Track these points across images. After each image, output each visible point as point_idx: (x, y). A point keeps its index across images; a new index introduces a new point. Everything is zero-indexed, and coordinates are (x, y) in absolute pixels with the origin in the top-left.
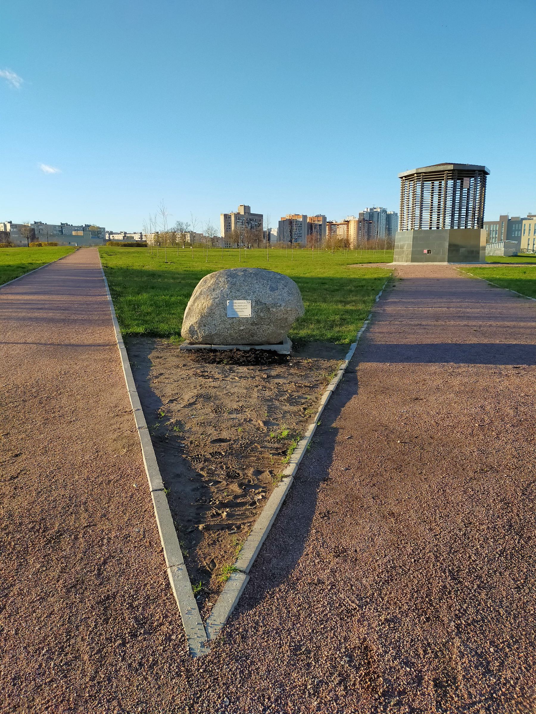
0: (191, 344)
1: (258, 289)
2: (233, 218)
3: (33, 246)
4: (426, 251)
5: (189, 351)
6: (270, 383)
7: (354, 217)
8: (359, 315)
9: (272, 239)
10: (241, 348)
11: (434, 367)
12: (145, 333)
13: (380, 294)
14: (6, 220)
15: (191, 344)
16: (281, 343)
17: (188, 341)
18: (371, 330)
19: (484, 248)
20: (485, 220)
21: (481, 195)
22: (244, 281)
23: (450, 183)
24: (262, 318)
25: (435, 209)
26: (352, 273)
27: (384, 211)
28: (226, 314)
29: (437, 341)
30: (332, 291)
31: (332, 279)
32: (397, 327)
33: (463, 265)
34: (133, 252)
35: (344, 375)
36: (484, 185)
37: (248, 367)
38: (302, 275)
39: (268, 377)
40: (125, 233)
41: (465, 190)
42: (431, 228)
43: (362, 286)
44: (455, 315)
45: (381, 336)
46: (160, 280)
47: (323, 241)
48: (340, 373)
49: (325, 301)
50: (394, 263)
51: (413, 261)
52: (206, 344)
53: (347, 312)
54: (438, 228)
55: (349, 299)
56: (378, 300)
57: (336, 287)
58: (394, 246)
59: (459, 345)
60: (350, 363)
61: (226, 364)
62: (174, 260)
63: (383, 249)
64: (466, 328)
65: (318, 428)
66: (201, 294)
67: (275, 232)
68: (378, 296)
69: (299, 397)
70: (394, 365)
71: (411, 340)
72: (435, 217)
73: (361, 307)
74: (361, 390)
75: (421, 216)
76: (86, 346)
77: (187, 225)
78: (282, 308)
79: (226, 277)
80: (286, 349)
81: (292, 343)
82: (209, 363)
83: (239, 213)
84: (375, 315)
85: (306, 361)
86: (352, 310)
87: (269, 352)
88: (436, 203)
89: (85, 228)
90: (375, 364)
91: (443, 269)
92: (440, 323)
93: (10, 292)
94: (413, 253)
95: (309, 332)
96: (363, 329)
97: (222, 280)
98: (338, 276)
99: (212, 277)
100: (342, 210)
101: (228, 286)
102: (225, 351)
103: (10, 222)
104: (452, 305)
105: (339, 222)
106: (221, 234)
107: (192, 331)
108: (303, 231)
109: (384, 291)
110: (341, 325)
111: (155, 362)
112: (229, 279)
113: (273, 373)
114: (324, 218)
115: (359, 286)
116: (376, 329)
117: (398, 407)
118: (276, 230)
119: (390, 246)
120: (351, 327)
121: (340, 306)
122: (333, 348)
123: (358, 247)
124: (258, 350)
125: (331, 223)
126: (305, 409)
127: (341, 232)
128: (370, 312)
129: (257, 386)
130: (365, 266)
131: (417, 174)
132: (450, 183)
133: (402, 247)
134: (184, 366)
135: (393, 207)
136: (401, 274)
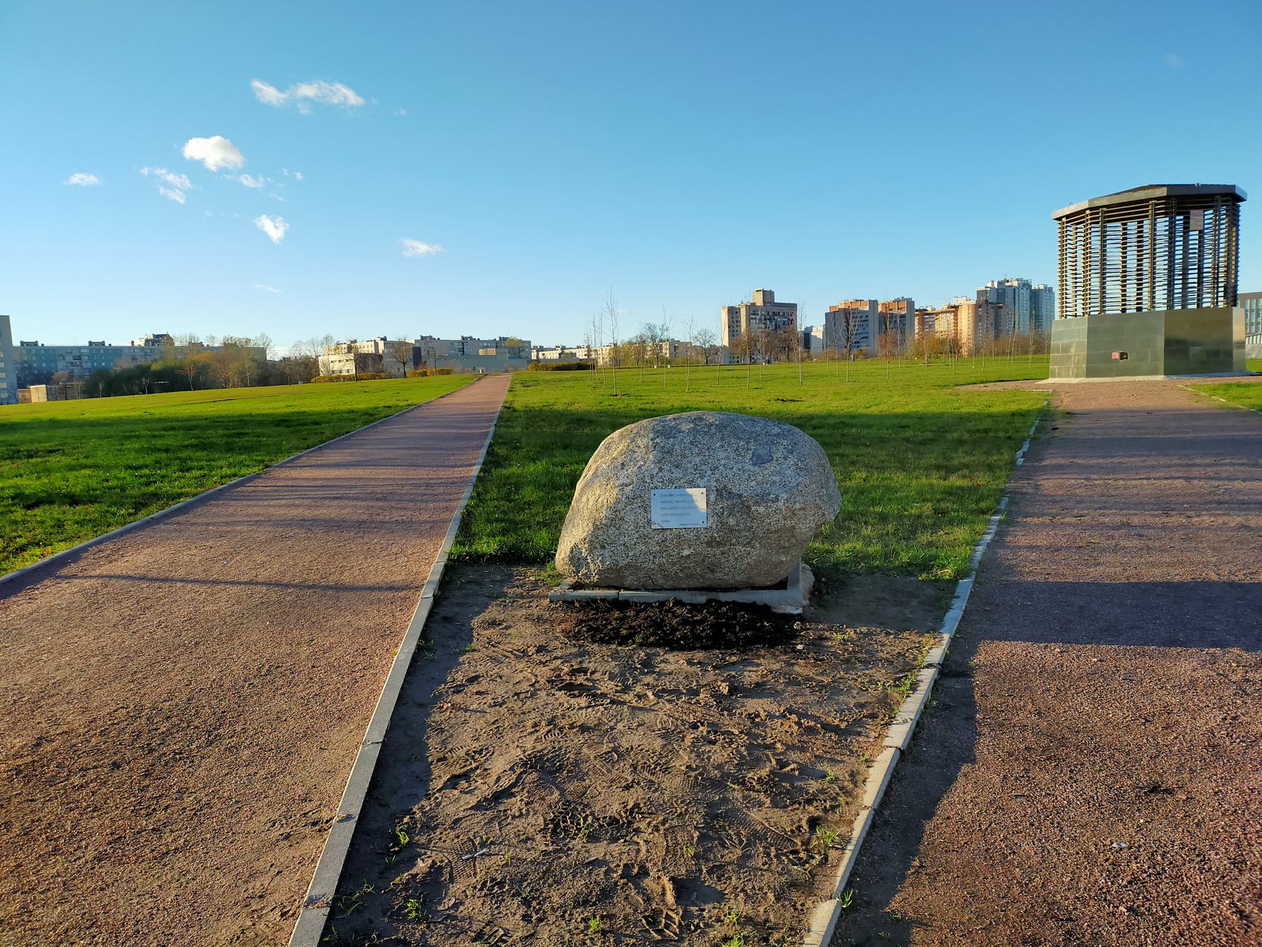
0: (576, 586)
1: (723, 462)
2: (743, 312)
3: (414, 375)
4: (1116, 355)
5: (569, 604)
6: (731, 715)
7: (967, 299)
8: (978, 501)
9: (813, 344)
10: (686, 597)
11: (1187, 664)
12: (496, 556)
13: (1026, 447)
14: (376, 336)
15: (576, 586)
16: (782, 585)
17: (571, 581)
18: (1009, 538)
19: (1242, 345)
20: (1240, 290)
21: (1229, 241)
22: (691, 443)
23: (1162, 224)
24: (731, 530)
25: (1132, 276)
26: (963, 403)
27: (1026, 285)
28: (649, 522)
29: (1179, 575)
30: (921, 443)
31: (920, 418)
32: (1070, 531)
33: (1199, 380)
34: (568, 380)
35: (936, 686)
36: (1234, 221)
37: (689, 655)
38: (861, 411)
39: (733, 690)
40: (564, 348)
41: (1194, 235)
42: (1124, 311)
43: (986, 431)
44: (1209, 498)
45: (1033, 556)
46: (587, 430)
47: (908, 343)
48: (927, 677)
49: (902, 467)
50: (1050, 380)
51: (1089, 375)
52: (609, 587)
53: (950, 492)
54: (1139, 309)
55: (956, 462)
56: (1020, 461)
57: (930, 435)
58: (1049, 347)
59: (1241, 586)
60: (954, 641)
61: (641, 645)
62: (632, 391)
63: (1027, 353)
64: (1247, 534)
65: (843, 918)
66: (595, 475)
67: (818, 333)
68: (1020, 453)
69: (805, 771)
70: (1073, 650)
71: (1110, 569)
72: (1132, 291)
73: (982, 479)
74: (984, 746)
75: (1103, 288)
76: (371, 589)
77: (665, 329)
78: (780, 504)
79: (651, 435)
80: (791, 602)
81: (813, 578)
82: (602, 641)
83: (754, 304)
84: (1015, 498)
85: (840, 637)
86: (962, 489)
87: (751, 607)
88: (1132, 264)
89: (500, 343)
90: (1019, 648)
91: (1154, 389)
92: (1176, 519)
93: (313, 462)
94: (1090, 359)
95: (859, 545)
96: (988, 538)
97: (642, 442)
98: (934, 409)
99: (622, 436)
100: (944, 283)
101: (655, 456)
102: (649, 605)
103: (384, 339)
104: (1195, 472)
105: (938, 309)
106: (722, 339)
107: (575, 559)
108: (869, 329)
109: (1034, 439)
110: (935, 527)
111: (481, 635)
112: (658, 440)
113: (750, 676)
114: (910, 303)
115: (978, 431)
116: (1020, 538)
117: (1103, 826)
118: (821, 329)
119: (1041, 346)
120: (960, 533)
121: (935, 480)
122: (912, 596)
123: (976, 352)
124: (727, 603)
125: (923, 312)
126: (814, 823)
127: (943, 326)
128: (1003, 492)
129: (694, 727)
130: (991, 386)
131: (1090, 209)
132: (1162, 224)
133: (1066, 349)
134: (538, 652)
135: (1044, 275)
136: (1066, 403)
